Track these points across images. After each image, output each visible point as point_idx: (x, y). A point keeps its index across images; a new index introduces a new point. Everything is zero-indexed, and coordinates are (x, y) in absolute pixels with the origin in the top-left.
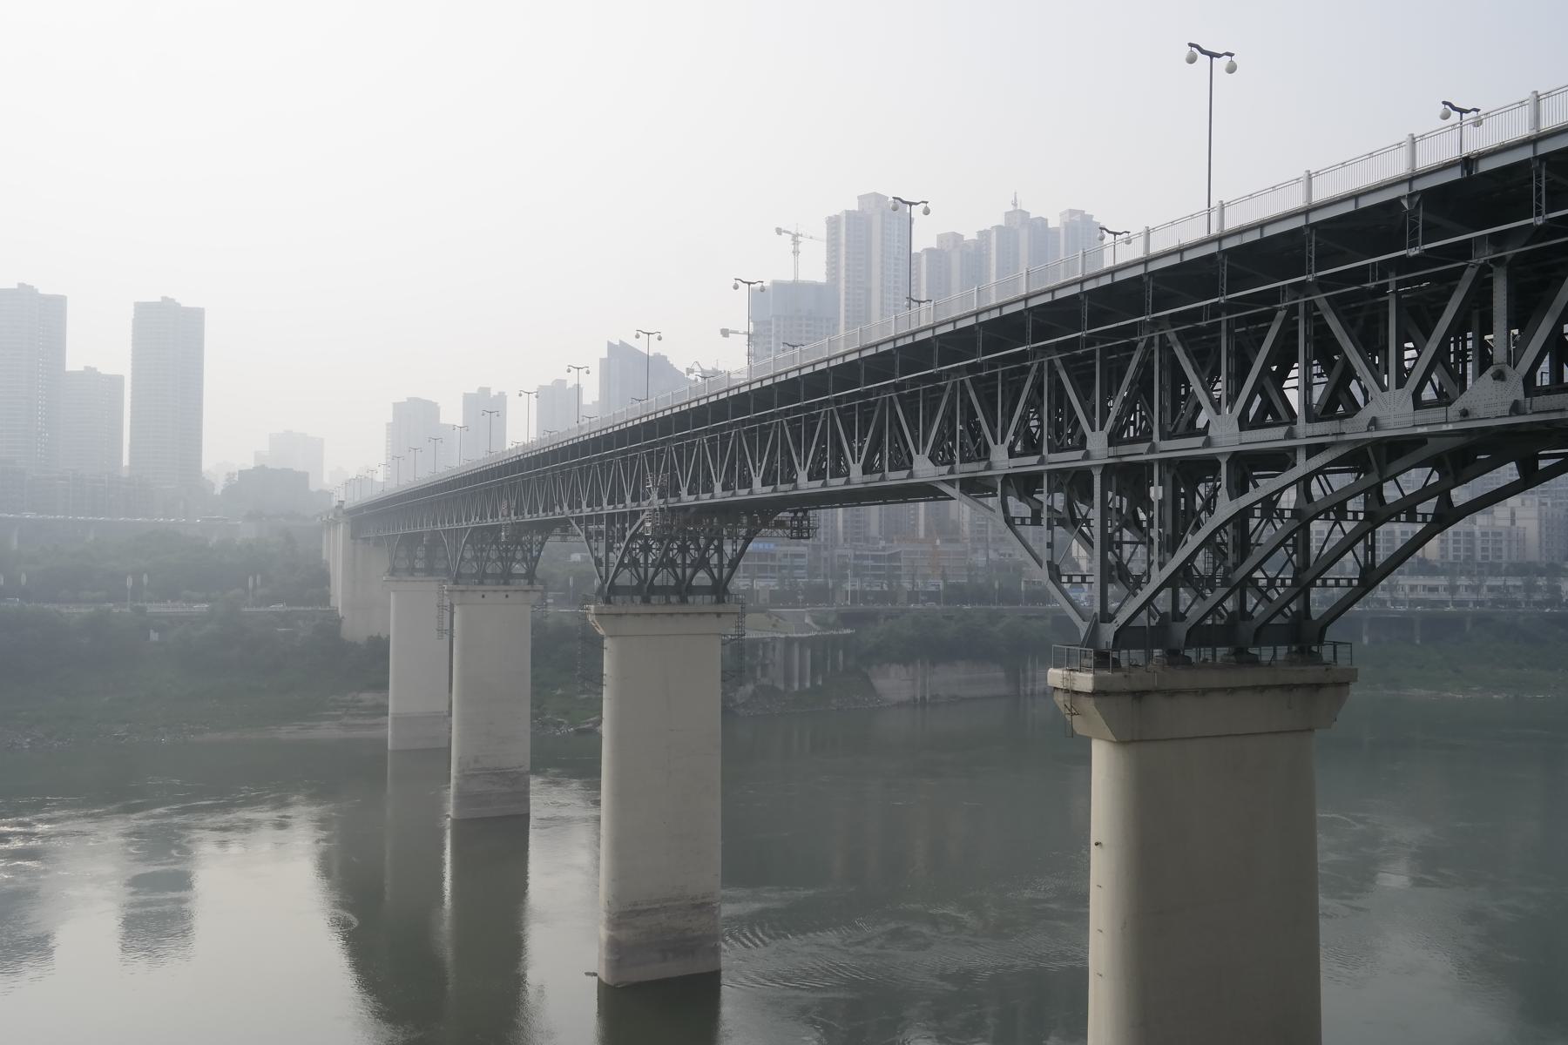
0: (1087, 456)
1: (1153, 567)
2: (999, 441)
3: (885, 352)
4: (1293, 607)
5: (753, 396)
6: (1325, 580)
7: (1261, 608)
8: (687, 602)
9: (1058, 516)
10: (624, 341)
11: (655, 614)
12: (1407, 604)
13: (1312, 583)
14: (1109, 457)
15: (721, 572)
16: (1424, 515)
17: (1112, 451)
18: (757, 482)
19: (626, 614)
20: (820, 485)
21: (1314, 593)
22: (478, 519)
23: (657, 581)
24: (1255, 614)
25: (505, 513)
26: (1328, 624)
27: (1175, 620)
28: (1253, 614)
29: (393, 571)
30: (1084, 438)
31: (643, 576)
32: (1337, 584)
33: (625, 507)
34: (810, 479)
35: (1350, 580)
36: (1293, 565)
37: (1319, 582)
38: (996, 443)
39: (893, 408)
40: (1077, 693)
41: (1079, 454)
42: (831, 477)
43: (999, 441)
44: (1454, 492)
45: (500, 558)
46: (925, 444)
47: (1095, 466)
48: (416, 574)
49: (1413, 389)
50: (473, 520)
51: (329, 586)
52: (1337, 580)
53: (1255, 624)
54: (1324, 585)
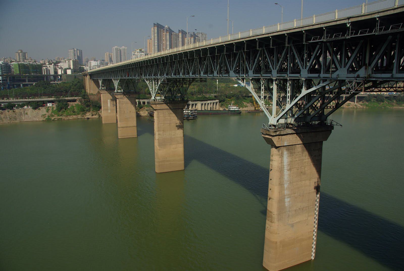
1: (203, 105)
2: (274, 68)
4: (320, 112)
6: (327, 107)
7: (313, 112)
10: (183, 30)
13: (324, 108)
16: (335, 92)
17: (279, 75)
18: (181, 74)
21: (325, 110)
24: (311, 114)
26: (328, 116)
27: (308, 115)
28: (311, 114)
30: (271, 71)
32: (330, 108)
35: (333, 106)
36: (320, 103)
37: (326, 107)
39: (209, 58)
43: (274, 68)
44: (342, 88)
46: (232, 68)
49: (347, 68)
51: (302, 89)
52: (330, 107)
53: (311, 117)
54: (327, 108)
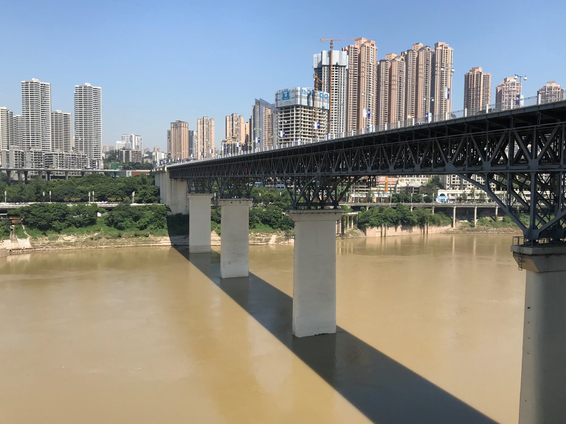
0: (305, 174)
3: (395, 133)
5: (387, 137)
8: (324, 208)
9: (528, 187)
11: (313, 213)
12: (30, 177)
14: (539, 169)
15: (336, 198)
19: (303, 213)
20: (526, 168)
22: (232, 174)
23: (314, 201)
25: (246, 173)
29: (190, 191)
31: (294, 198)
33: (305, 174)
34: (336, 171)
38: (417, 164)
40: (524, 254)
41: (526, 167)
42: (313, 172)
45: (195, 186)
47: (532, 172)
48: (191, 192)
50: (230, 174)
